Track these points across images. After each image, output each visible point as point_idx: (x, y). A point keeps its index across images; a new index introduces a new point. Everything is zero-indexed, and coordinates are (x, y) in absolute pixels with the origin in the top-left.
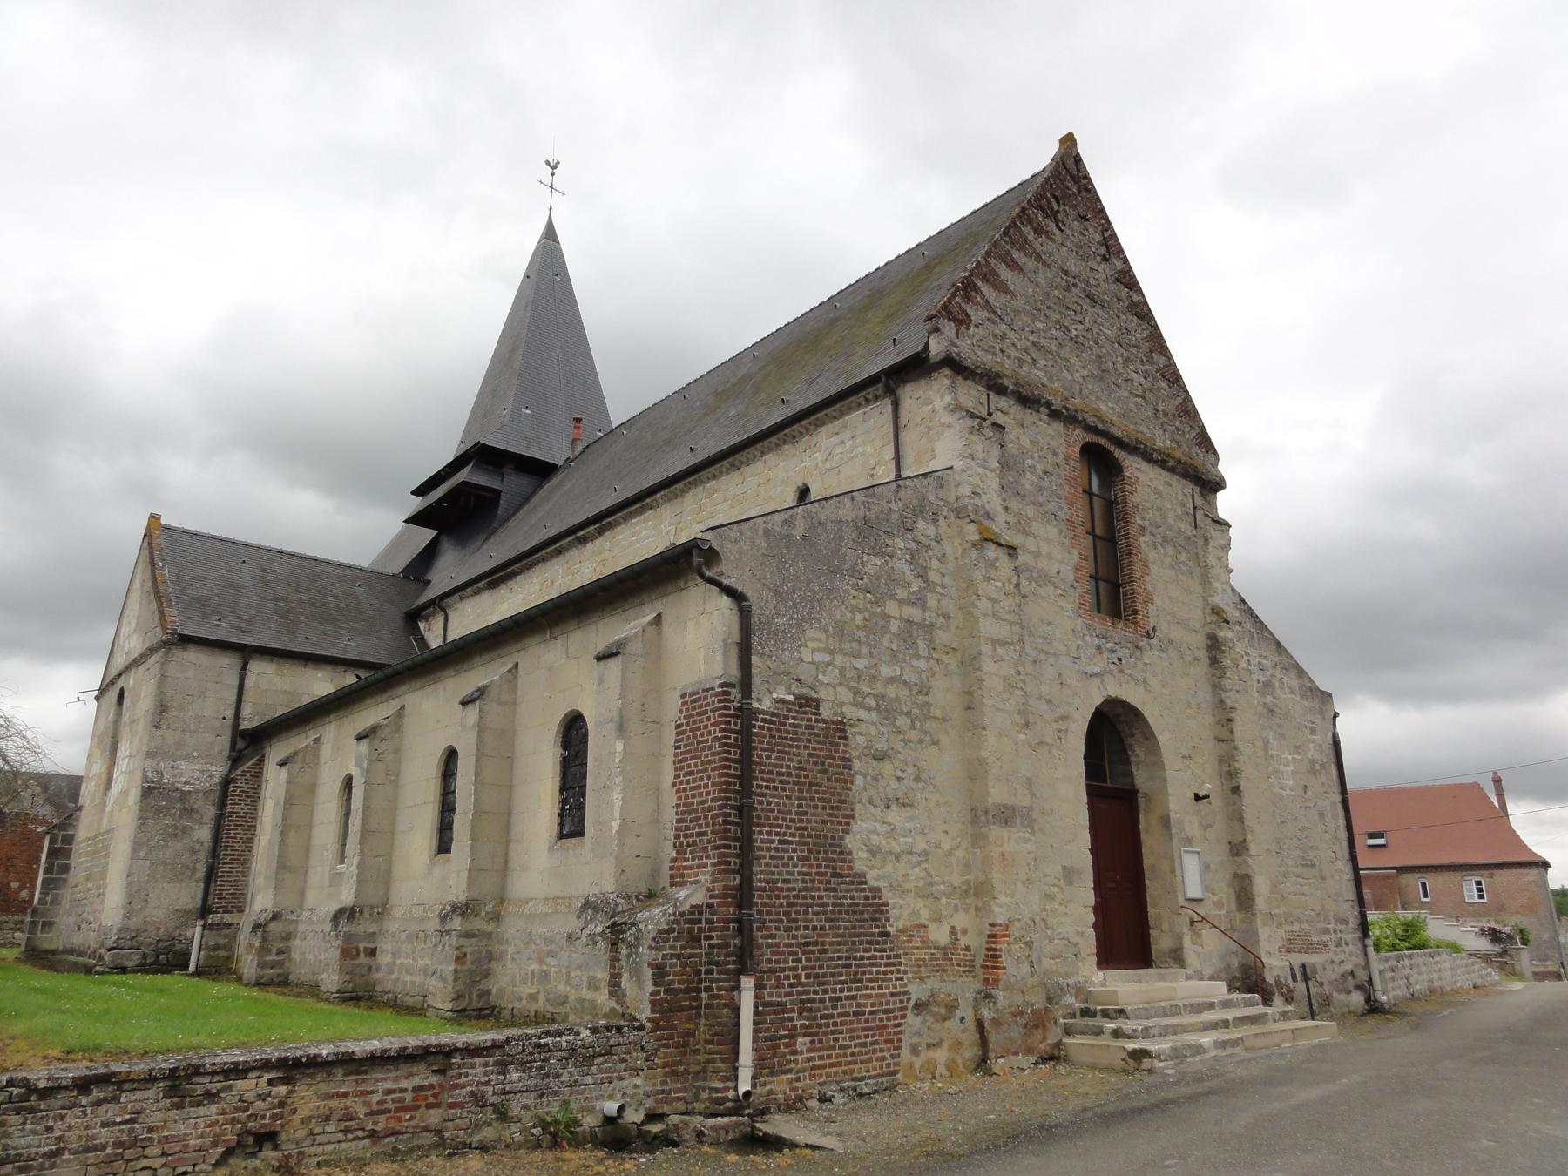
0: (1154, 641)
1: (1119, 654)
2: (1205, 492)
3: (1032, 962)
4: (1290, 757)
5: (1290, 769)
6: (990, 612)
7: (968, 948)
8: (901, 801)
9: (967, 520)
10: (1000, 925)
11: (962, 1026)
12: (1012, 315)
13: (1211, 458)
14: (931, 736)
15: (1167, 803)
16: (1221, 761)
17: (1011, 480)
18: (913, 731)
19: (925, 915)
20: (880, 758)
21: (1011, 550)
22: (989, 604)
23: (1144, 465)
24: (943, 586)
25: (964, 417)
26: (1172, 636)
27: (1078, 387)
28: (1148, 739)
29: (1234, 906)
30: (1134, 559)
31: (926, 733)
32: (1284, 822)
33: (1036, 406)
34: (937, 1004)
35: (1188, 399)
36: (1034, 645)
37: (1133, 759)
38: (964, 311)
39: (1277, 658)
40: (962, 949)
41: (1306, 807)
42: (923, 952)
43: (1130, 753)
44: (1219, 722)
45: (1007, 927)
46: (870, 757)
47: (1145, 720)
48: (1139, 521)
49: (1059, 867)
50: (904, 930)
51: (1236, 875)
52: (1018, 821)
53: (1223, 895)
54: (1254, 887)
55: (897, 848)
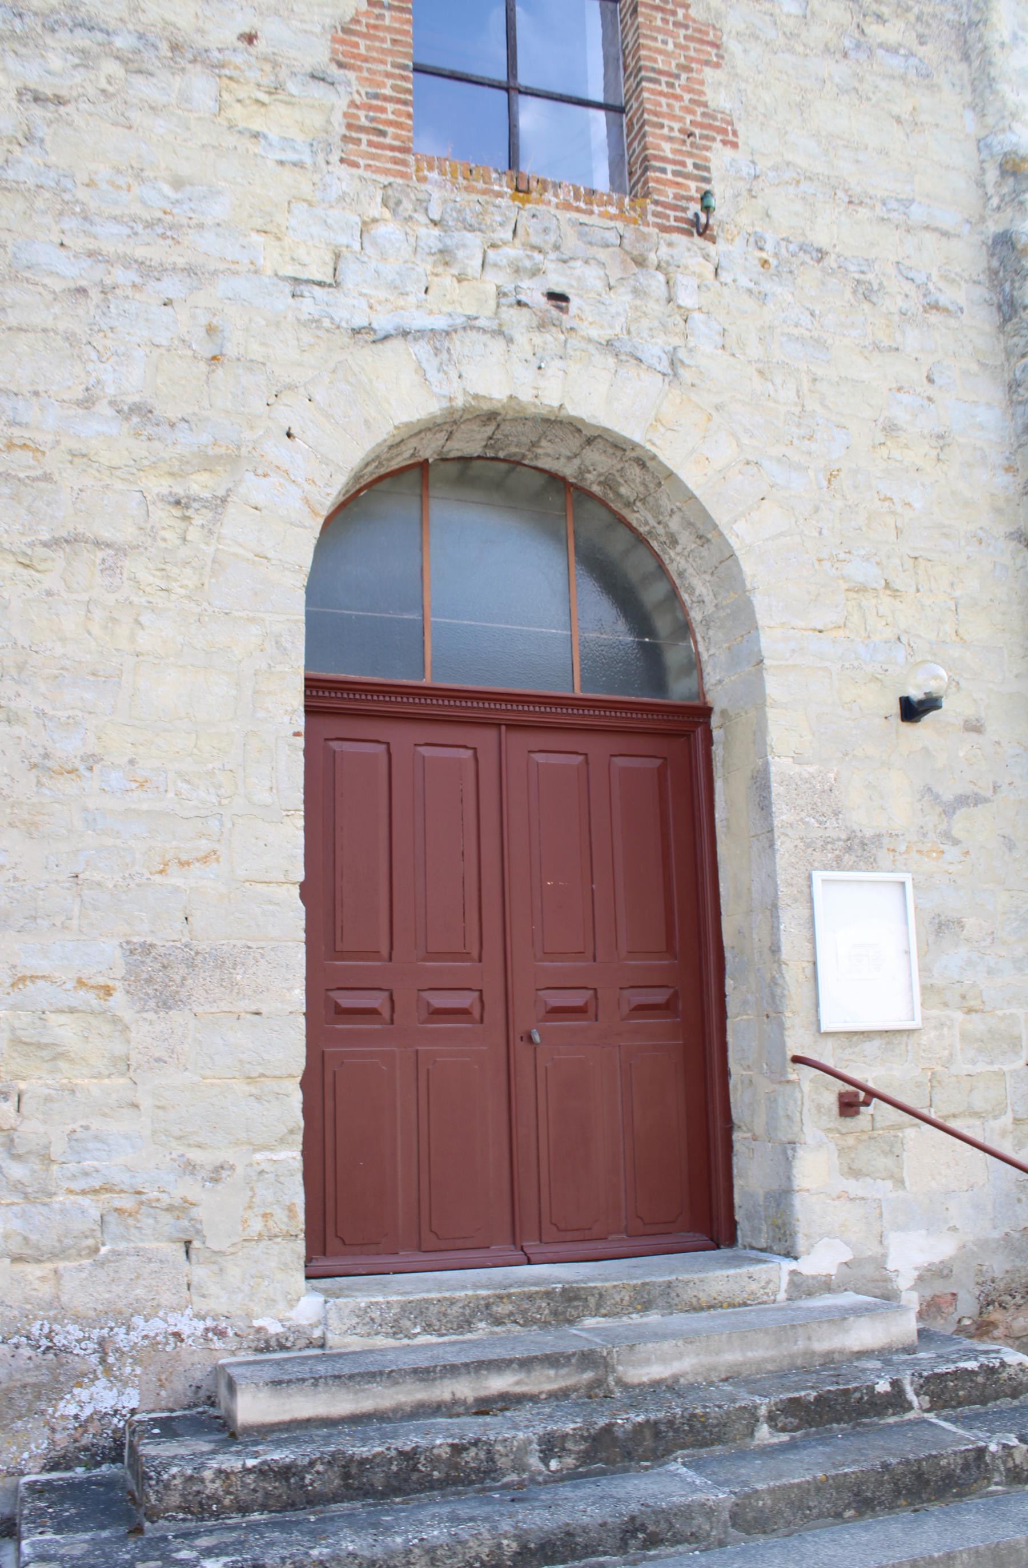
26: (821, 239)
36: (78, 243)
37: (696, 615)
43: (685, 597)
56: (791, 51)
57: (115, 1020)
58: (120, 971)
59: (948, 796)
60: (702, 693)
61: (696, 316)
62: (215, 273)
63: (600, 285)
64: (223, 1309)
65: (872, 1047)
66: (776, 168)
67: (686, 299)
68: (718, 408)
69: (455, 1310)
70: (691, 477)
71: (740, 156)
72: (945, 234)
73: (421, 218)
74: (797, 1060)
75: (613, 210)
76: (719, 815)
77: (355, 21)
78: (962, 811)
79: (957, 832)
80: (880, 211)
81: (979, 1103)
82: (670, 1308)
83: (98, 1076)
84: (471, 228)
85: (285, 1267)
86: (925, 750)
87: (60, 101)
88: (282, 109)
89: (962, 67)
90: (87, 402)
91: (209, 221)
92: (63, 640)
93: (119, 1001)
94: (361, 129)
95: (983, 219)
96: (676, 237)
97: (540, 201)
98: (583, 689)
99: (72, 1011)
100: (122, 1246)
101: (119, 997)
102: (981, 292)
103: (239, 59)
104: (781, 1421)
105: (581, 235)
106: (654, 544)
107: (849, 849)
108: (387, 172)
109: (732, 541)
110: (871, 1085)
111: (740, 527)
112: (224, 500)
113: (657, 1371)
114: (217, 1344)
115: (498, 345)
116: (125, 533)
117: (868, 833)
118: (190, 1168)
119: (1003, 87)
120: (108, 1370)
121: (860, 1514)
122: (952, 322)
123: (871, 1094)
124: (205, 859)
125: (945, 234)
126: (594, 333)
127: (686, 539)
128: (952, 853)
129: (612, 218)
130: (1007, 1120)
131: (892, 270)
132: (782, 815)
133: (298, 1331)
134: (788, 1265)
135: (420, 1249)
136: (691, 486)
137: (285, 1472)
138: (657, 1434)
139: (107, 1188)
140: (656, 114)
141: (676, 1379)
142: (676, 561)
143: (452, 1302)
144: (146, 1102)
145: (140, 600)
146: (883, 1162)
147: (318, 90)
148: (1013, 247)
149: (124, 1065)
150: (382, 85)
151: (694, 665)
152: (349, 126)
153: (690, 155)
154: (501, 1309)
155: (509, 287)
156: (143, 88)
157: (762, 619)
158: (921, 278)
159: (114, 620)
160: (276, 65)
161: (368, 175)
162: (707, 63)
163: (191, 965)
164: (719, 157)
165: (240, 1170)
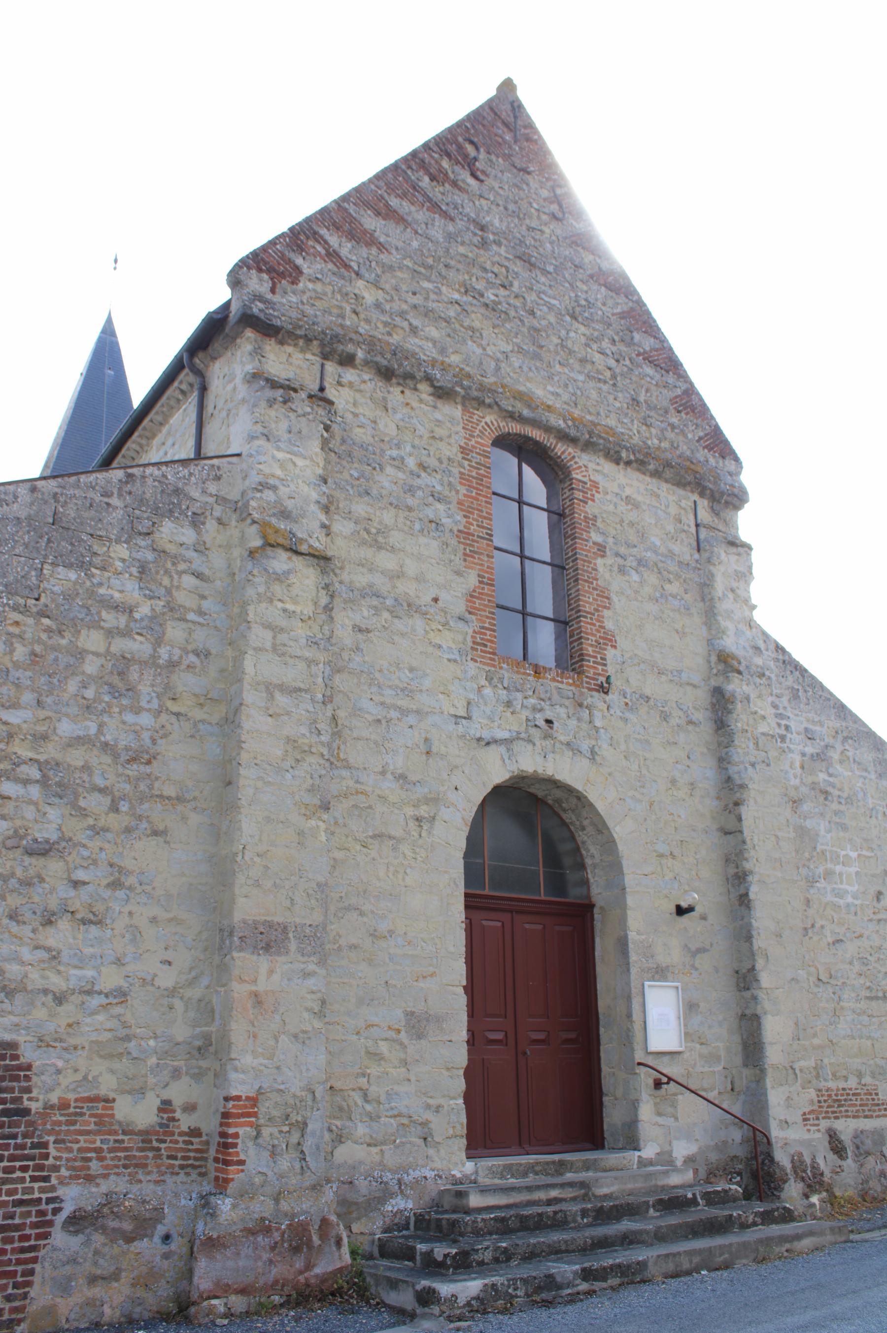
0: (612, 697)
1: (549, 715)
2: (717, 507)
3: (302, 1152)
4: (854, 855)
5: (853, 870)
6: (268, 645)
7: (195, 1132)
8: (79, 916)
9: (249, 521)
10: (238, 1098)
11: (165, 1248)
12: (379, 271)
13: (730, 465)
14: (149, 822)
15: (623, 920)
16: (727, 861)
17: (356, 474)
18: (112, 815)
19: (107, 1085)
20: (42, 850)
21: (321, 559)
22: (268, 635)
23: (608, 467)
24: (201, 612)
25: (263, 388)
26: (648, 691)
27: (493, 364)
28: (600, 832)
29: (738, 1060)
30: (583, 586)
31: (140, 818)
32: (840, 941)
33: (410, 383)
34: (117, 1216)
35: (690, 391)
36: (377, 698)
37: (588, 861)
38: (290, 262)
39: (837, 724)
40: (181, 1134)
41: (879, 921)
42: (98, 1138)
43: (584, 852)
44: (726, 808)
45: (254, 1101)
46: (19, 851)
47: (591, 805)
48: (595, 537)
49: (399, 1013)
50: (64, 1105)
51: (743, 1016)
52: (293, 946)
53: (721, 1045)
54: (764, 1033)
55: (56, 982)
56: (636, 599)
57: (401, 1044)
58: (403, 1023)
59: (693, 949)
60: (589, 897)
61: (602, 731)
62: (427, 713)
63: (565, 716)
64: (440, 1167)
65: (666, 1059)
66: (630, 658)
67: (598, 723)
68: (610, 774)
69: (522, 1168)
70: (600, 806)
71: (617, 652)
72: (695, 686)
73: (500, 686)
74: (639, 1064)
75: (571, 681)
76: (598, 953)
77: (474, 591)
78: (699, 956)
79: (697, 965)
80: (670, 677)
81: (706, 1086)
82: (596, 1170)
83: (395, 1067)
84: (518, 690)
85: (460, 1149)
86: (685, 928)
87: (368, 631)
88: (447, 632)
89: (701, 604)
90: (383, 773)
91: (424, 689)
92: (379, 880)
93: (403, 1035)
94: (478, 644)
95: (709, 678)
96: (595, 693)
97: (544, 678)
98: (545, 895)
99: (386, 1039)
100: (404, 1140)
101: (403, 1033)
102: (708, 714)
103: (432, 611)
104: (657, 1207)
105: (559, 693)
106: (572, 828)
107: (657, 972)
108: (488, 664)
109: (615, 835)
110: (670, 1075)
111: (618, 829)
112: (434, 818)
113: (605, 1191)
114: (439, 1182)
115: (530, 747)
116: (398, 832)
117: (664, 965)
118: (428, 1107)
119: (719, 618)
120: (402, 1192)
121: (693, 1238)
122: (698, 729)
123: (670, 1079)
124: (431, 976)
125: (695, 686)
126: (562, 738)
127: (590, 830)
128: (695, 974)
129: (571, 685)
130: (716, 1092)
131: (674, 705)
132: (633, 957)
133: (466, 1176)
134: (637, 1153)
135: (485, 1147)
136: (600, 810)
137: (503, 1220)
138: (617, 1211)
139: (400, 1115)
140: (587, 633)
141: (612, 1194)
142: (581, 837)
143: (521, 1165)
144: (413, 1079)
145: (406, 863)
146: (670, 1110)
147: (461, 624)
148: (723, 696)
149: (404, 1063)
150: (484, 622)
151: (585, 883)
152: (474, 643)
153: (599, 653)
154: (537, 1168)
155: (531, 717)
156: (399, 625)
157: (626, 871)
158: (685, 708)
159: (397, 871)
160: (446, 613)
161: (481, 666)
162: (605, 607)
163: (428, 1021)
164: (610, 653)
165: (446, 1108)
